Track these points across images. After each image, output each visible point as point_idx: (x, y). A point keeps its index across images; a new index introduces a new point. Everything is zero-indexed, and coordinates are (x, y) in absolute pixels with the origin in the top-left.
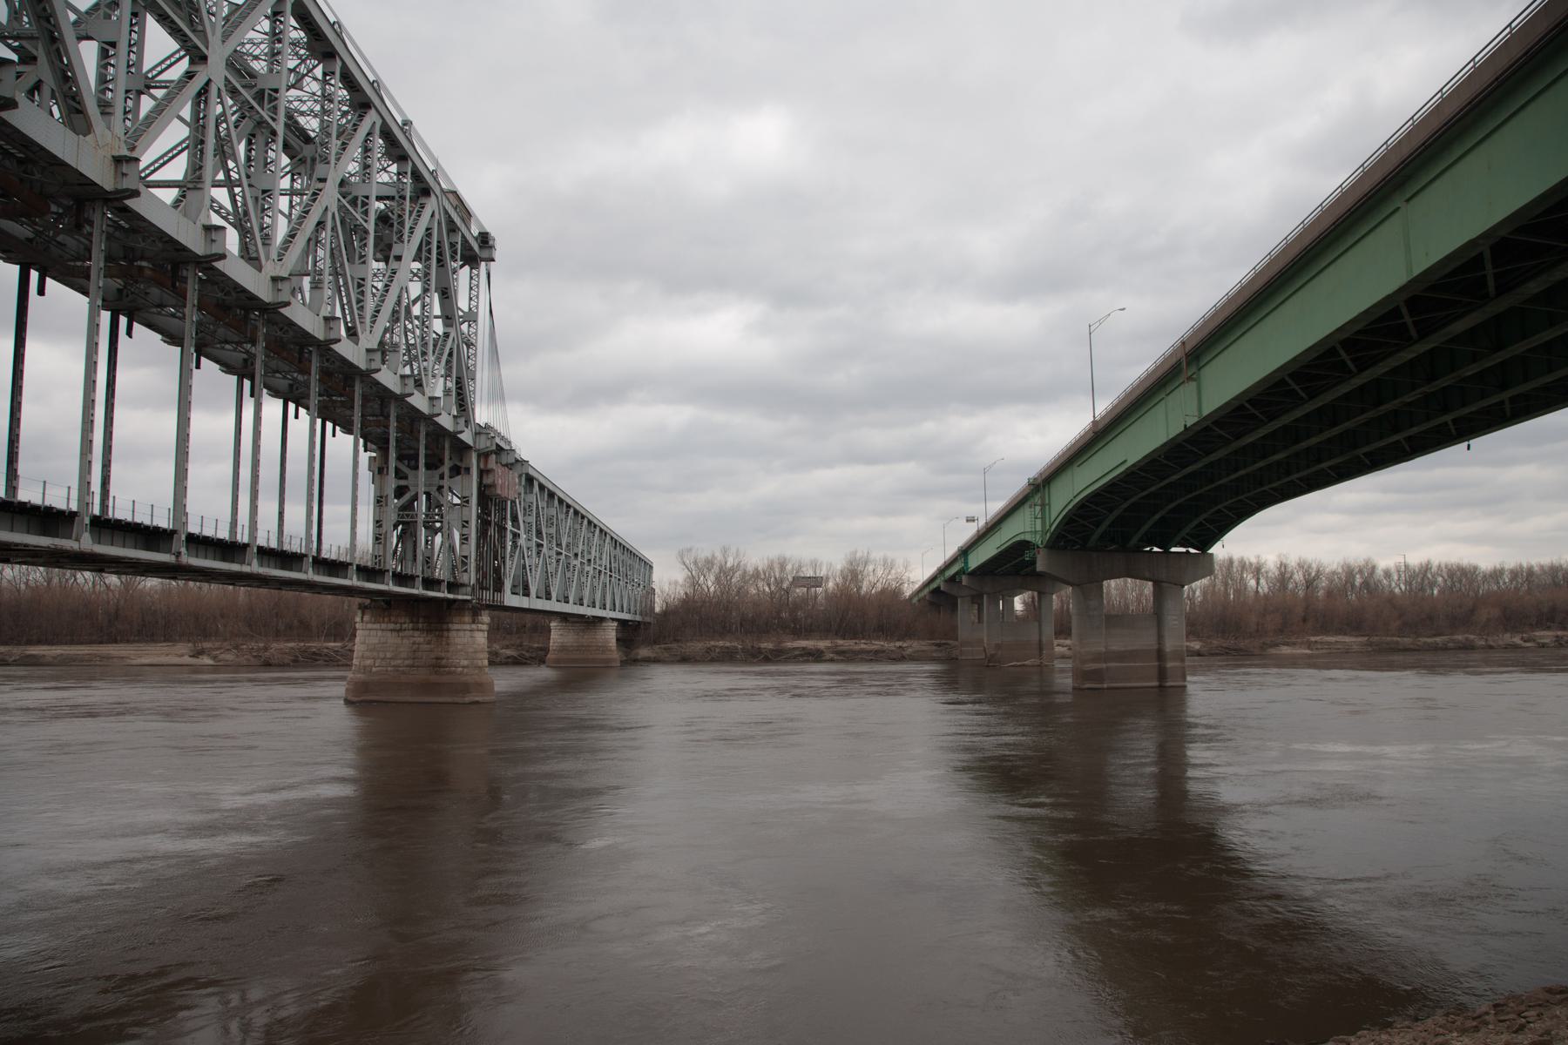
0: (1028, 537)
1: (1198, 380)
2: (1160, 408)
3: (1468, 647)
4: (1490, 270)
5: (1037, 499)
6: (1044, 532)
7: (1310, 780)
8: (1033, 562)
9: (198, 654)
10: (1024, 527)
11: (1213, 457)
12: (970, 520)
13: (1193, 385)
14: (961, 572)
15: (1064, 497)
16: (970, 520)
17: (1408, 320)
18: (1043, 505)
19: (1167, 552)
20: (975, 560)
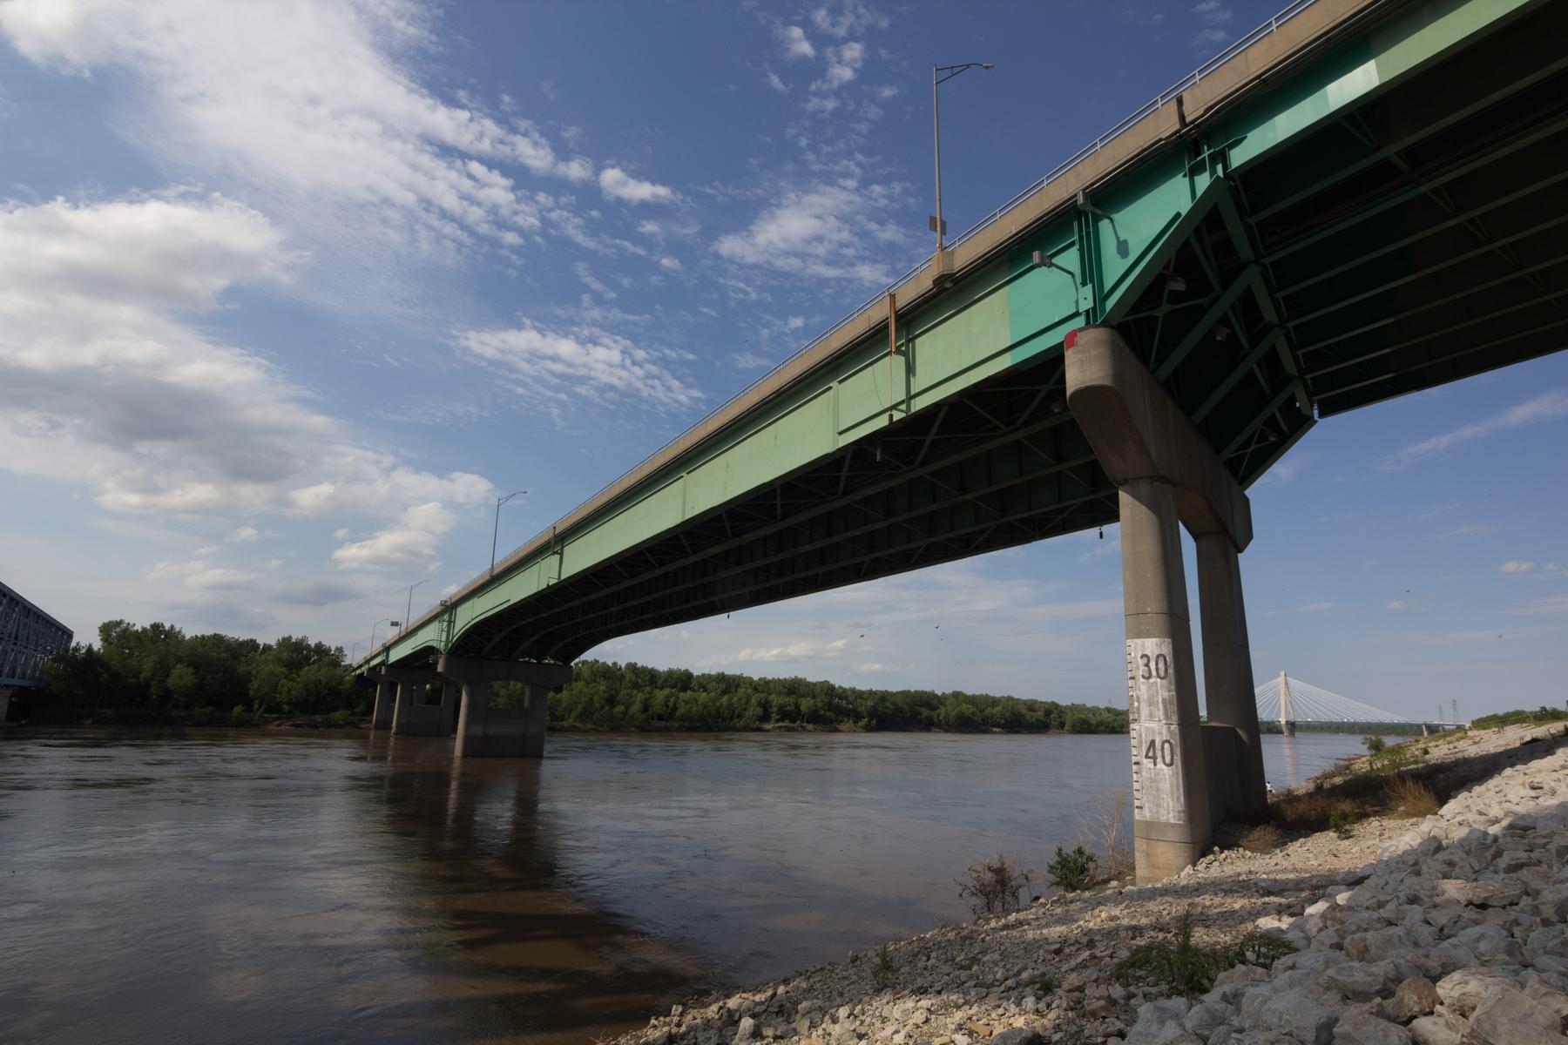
0: (434, 644)
1: (561, 555)
2: (536, 568)
3: (666, 729)
4: (779, 502)
5: (446, 617)
6: (447, 642)
7: (613, 819)
8: (436, 663)
9: (1397, 749)
10: (432, 636)
11: (571, 605)
12: (394, 624)
13: (557, 557)
14: (382, 663)
15: (468, 616)
16: (394, 624)
17: (779, 502)
18: (450, 622)
19: (540, 662)
20: (396, 655)
